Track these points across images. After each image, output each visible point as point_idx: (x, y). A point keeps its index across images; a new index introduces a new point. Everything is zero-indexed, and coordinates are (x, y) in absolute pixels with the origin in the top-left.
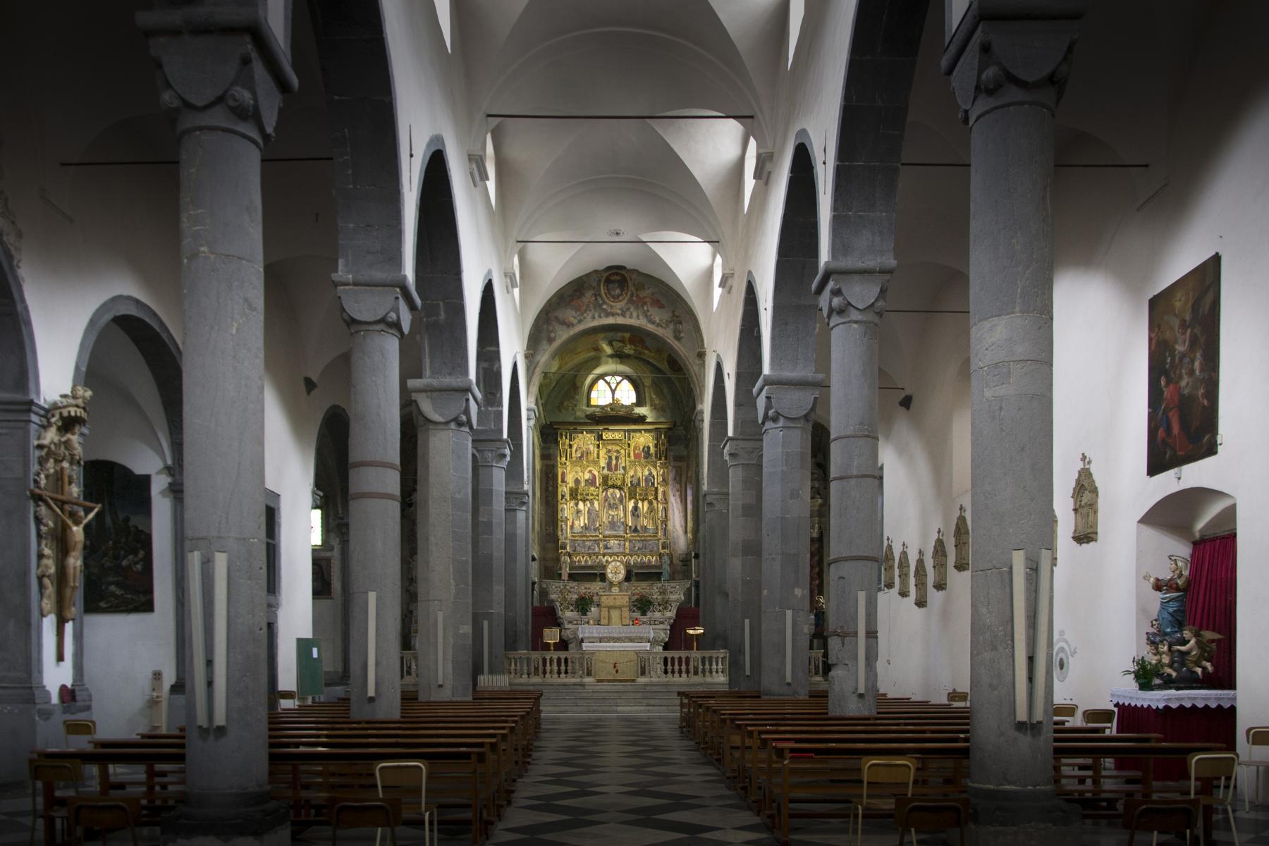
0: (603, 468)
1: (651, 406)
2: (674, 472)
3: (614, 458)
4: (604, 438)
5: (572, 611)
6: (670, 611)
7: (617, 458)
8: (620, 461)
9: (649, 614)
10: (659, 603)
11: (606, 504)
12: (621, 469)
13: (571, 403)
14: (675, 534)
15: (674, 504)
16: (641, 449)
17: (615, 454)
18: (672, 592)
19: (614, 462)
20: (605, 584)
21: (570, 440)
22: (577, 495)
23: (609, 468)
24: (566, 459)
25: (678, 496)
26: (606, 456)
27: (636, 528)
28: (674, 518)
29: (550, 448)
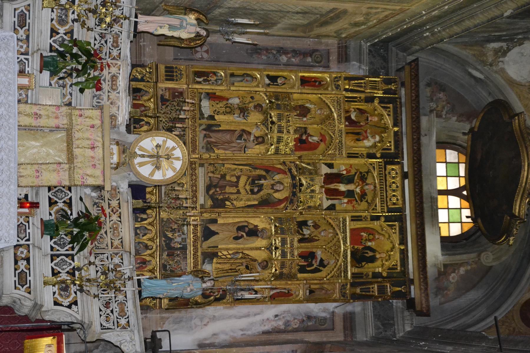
0: (330, 166)
1: (445, 266)
2: (324, 315)
3: (351, 187)
4: (389, 167)
5: (54, 32)
6: (56, 303)
7: (350, 194)
8: (346, 200)
9: (47, 242)
10: (79, 269)
11: (259, 172)
12: (330, 202)
13: (443, 107)
14: (197, 321)
15: (259, 318)
16: (369, 244)
17: (358, 190)
18: (107, 305)
19: (343, 188)
20: (123, 129)
21: (382, 100)
22: (278, 107)
23: (330, 178)
24: (346, 90)
25: (274, 324)
26: (353, 172)
27: (214, 233)
28: (230, 317)
29: (360, 61)
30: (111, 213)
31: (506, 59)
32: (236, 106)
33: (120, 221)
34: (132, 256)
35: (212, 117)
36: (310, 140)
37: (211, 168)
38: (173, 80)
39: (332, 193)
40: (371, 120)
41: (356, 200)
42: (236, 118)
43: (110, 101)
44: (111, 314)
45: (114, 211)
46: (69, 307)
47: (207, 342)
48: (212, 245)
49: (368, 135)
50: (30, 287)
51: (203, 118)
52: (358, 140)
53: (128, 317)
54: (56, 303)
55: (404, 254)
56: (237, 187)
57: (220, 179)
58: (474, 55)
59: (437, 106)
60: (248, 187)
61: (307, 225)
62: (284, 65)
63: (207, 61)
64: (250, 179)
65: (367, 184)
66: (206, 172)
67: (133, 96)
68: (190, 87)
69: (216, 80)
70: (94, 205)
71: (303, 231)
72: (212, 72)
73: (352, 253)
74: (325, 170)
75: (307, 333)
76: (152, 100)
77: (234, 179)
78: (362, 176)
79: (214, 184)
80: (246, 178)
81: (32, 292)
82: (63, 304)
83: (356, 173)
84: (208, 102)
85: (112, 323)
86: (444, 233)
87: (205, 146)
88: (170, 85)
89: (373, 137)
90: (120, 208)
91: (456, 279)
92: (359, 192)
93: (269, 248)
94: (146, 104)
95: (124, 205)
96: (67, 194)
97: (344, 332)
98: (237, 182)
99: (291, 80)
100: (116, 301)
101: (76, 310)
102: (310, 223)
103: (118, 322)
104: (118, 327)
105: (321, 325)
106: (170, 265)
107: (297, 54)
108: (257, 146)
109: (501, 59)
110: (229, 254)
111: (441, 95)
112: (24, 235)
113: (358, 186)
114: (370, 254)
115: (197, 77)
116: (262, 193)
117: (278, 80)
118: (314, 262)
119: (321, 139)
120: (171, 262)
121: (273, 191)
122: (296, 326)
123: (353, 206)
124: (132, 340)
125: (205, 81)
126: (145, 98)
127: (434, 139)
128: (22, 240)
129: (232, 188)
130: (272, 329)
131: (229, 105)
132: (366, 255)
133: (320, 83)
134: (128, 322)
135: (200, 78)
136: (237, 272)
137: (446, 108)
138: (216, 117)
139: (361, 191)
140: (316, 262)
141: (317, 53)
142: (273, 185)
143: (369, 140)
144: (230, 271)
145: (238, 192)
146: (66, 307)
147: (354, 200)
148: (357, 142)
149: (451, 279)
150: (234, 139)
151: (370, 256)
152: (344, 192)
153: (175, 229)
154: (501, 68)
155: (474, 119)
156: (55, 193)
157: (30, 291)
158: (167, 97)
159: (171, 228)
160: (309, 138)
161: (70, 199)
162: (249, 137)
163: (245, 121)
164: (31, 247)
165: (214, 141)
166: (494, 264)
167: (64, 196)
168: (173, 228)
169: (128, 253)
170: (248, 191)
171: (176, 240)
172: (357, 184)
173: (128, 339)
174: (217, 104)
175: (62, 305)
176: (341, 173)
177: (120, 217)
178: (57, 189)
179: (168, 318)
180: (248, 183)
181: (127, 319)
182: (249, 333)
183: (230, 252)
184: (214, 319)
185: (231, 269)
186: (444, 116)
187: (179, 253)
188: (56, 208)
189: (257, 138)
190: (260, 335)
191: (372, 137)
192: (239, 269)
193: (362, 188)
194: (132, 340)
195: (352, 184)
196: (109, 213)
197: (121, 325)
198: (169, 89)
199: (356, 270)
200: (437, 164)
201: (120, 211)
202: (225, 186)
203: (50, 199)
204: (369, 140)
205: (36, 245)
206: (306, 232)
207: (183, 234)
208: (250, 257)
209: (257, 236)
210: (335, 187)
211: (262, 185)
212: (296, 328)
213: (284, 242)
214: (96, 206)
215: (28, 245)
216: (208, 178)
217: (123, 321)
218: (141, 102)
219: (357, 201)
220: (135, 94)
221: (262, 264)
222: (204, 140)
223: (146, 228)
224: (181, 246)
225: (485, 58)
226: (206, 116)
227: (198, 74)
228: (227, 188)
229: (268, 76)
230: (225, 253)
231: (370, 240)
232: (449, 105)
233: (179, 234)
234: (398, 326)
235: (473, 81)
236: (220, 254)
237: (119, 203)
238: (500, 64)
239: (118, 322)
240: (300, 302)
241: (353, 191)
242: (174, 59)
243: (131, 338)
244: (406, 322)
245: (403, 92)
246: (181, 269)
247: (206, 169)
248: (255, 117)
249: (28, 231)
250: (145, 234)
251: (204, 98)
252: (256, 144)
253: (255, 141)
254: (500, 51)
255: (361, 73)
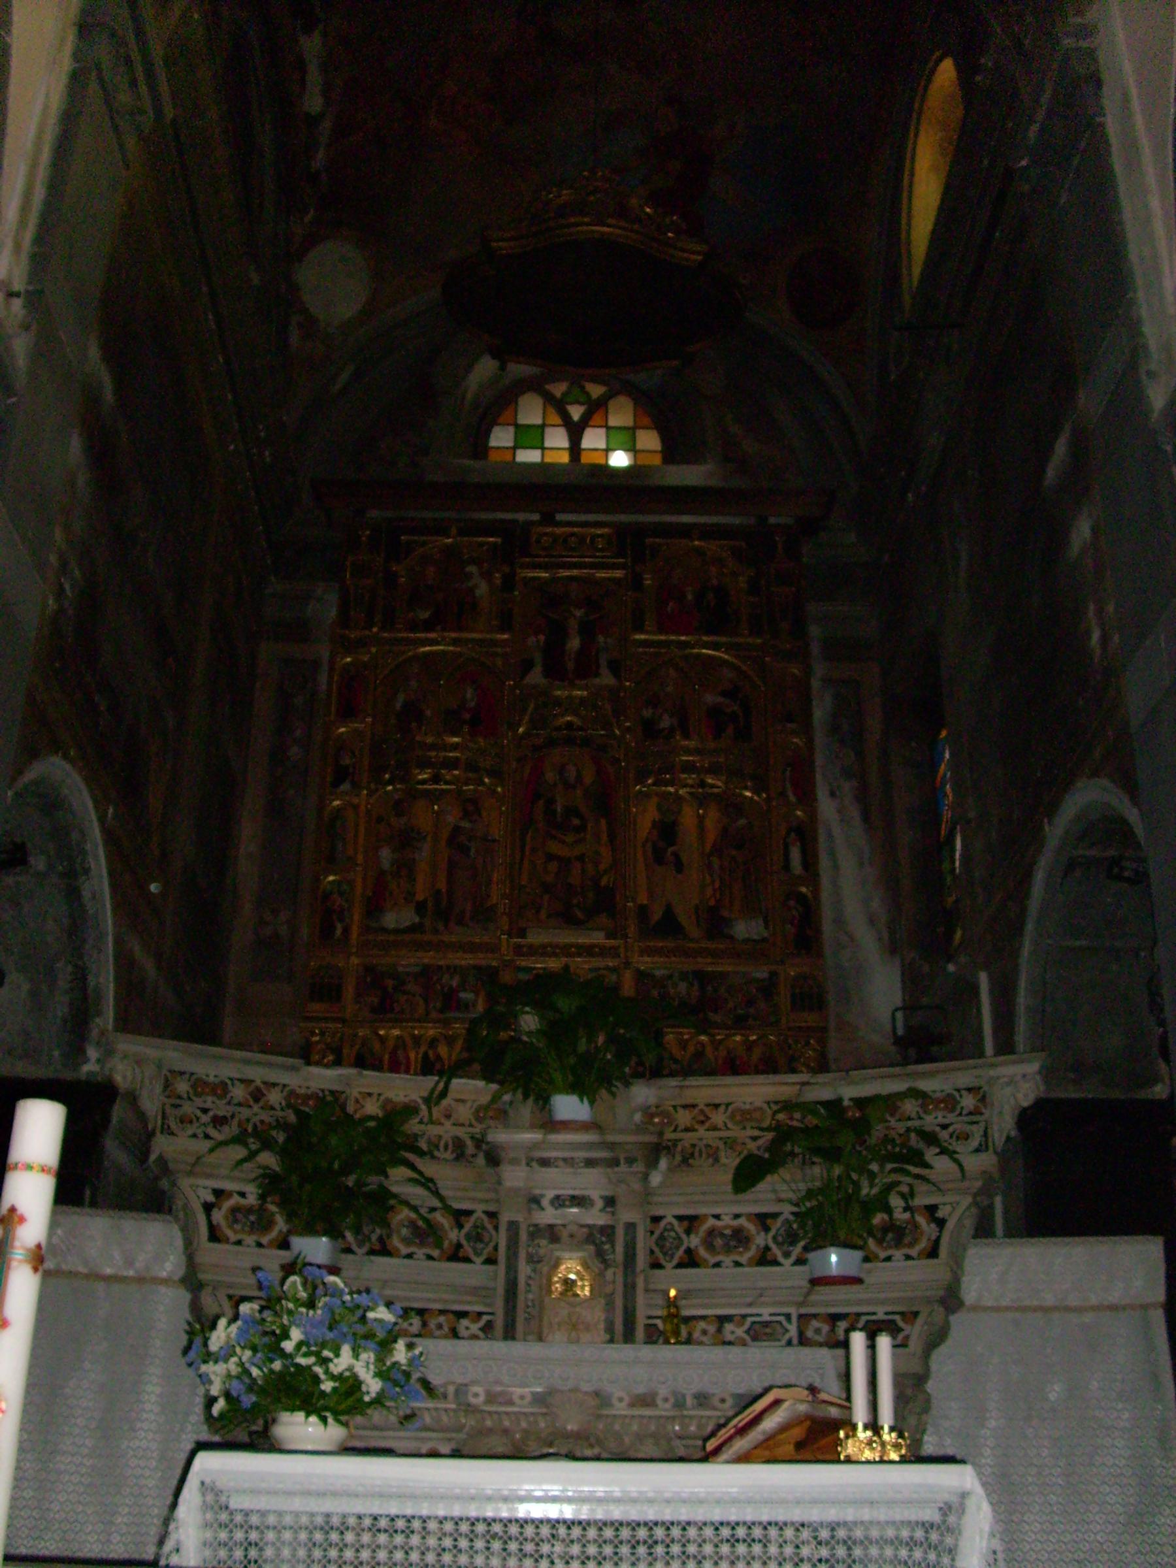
0: (527, 666)
6: (933, 1253)
7: (588, 631)
12: (604, 670)
17: (579, 613)
19: (574, 643)
23: (554, 671)
27: (669, 914)
30: (707, 1125)
33: (728, 1105)
34: (812, 1081)
35: (420, 908)
36: (473, 704)
39: (586, 668)
42: (423, 854)
43: (443, 1120)
44: (951, 1129)
45: (702, 1118)
46: (941, 1223)
47: (886, 936)
50: (902, 1314)
51: (421, 925)
53: (958, 1090)
54: (933, 1253)
55: (708, 532)
60: (570, 839)
68: (354, 950)
69: (341, 894)
70: (689, 1165)
71: (664, 729)
73: (709, 632)
74: (536, 677)
76: (382, 1032)
77: (553, 866)
81: (915, 1309)
82: (933, 1237)
85: (974, 1128)
86: (657, 460)
88: (349, 993)
89: (469, 576)
90: (694, 1106)
93: (702, 801)
94: (391, 1044)
95: (690, 1096)
96: (669, 1227)
98: (559, 859)
100: (920, 1118)
101: (948, 1208)
102: (647, 713)
103: (970, 1113)
104: (981, 1114)
108: (484, 814)
110: (713, 882)
112: (778, 1327)
120: (731, 1005)
122: (852, 754)
124: (1011, 1082)
125: (342, 920)
126: (377, 1046)
127: (469, 463)
128: (787, 1331)
134: (969, 1090)
138: (420, 897)
145: (581, 858)
146: (940, 1232)
156: (665, 1254)
157: (912, 1313)
161: (680, 1218)
163: (429, 839)
164: (803, 1311)
167: (673, 1234)
169: (804, 1088)
173: (1008, 1090)
175: (937, 1241)
176: (542, 644)
177: (717, 1106)
178: (657, 1250)
181: (964, 1093)
183: (708, 879)
184: (839, 921)
188: (702, 1252)
189: (466, 815)
194: (1011, 1082)
196: (708, 1130)
197: (976, 1107)
201: (701, 1106)
203: (680, 1265)
205: (801, 1299)
206: (666, 722)
207: (670, 977)
209: (674, 823)
213: (689, 768)
214: (690, 1161)
215: (801, 1316)
217: (968, 1102)
218: (387, 1057)
226: (417, 920)
227: (326, 931)
230: (709, 892)
236: (712, 903)
237: (685, 1107)
239: (970, 1113)
240: (810, 741)
243: (1008, 1084)
245: (374, 514)
248: (422, 817)
249: (766, 1318)
252: (480, 815)
255: (333, 597)
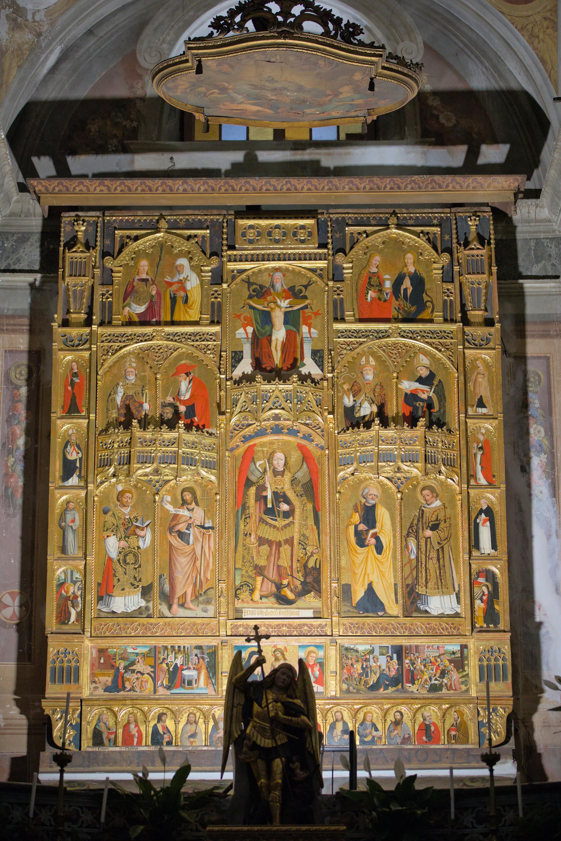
16: (388, 285)
17: (284, 304)
26: (248, 313)
27: (370, 591)
31: (29, 7)
32: (123, 543)
36: (187, 396)
37: (244, 595)
38: (77, 669)
40: (147, 274)
41: (302, 309)
48: (393, 595)
49: (176, 280)
52: (186, 300)
56: (279, 544)
57: (264, 576)
58: (19, 67)
59: (115, 136)
60: (281, 522)
61: (353, 407)
62: (36, 442)
63: (31, 596)
64: (265, 517)
65: (273, 286)
66: (251, 604)
67: (110, 746)
72: (59, 593)
75: (553, 409)
78: (257, 296)
79: (274, 589)
80: (262, 526)
83: (251, 307)
84: (117, 598)
87: (201, 606)
91: (449, 114)
92: (287, 301)
97: (552, 337)
98: (269, 543)
99: (70, 432)
105: (540, 382)
106: (430, 679)
107: (14, 415)
109: (30, 17)
111: (93, 128)
113: (275, 303)
114: (407, 284)
115: (69, 621)
116: (291, 494)
117: (70, 457)
118: (424, 396)
119: (184, 375)
120: (426, 677)
121: (287, 472)
122: (542, 430)
123: (316, 314)
129: (282, 555)
130: (547, 478)
131: (121, 557)
132: (409, 292)
133: (75, 375)
135: (70, 614)
136: (442, 547)
137: (118, 120)
139: (286, 298)
140: (423, 391)
141: (13, 374)
142: (276, 473)
143: (186, 279)
144: (441, 561)
145: (290, 541)
147: (304, 313)
148: (190, 302)
149: (450, 124)
150: (188, 549)
151: (411, 284)
152: (288, 332)
153: (362, 668)
154: (46, 16)
155: (140, 66)
158: (110, 679)
159: (360, 675)
160: (182, 398)
162: (183, 519)
165: (191, 587)
166: (420, 39)
168: (360, 671)
170: (287, 521)
171: (384, 667)
172: (272, 305)
174: (119, 580)
176: (250, 336)
179: (526, 679)
180: (273, 522)
182: (554, 522)
185: (438, 560)
186: (135, 124)
187: (407, 661)
190: (558, 502)
191: (180, 272)
192: (439, 543)
193: (278, 295)
195: (273, 314)
198: (93, 675)
199: (438, 315)
200: (224, 138)
202: (279, 567)
204: (186, 279)
207: (372, 651)
208: (415, 522)
210: (279, 348)
211: (275, 494)
212: (546, 434)
216: (264, 600)
218: (120, 731)
219: (306, 307)
220: (106, 741)
221: (427, 498)
222: (190, 609)
223: (361, 724)
224: (395, 656)
225: (26, 46)
226: (143, 603)
228: (281, 563)
229: (66, 476)
231: (381, 284)
232: (113, 114)
233: (371, 660)
234: (540, 232)
235: (67, 66)
236: (409, 581)
238: (37, 18)
241: (286, 314)
242: (30, 660)
244: (532, 216)
246: (439, 656)
247: (245, 605)
250: (374, 725)
251: (108, 605)
253: (191, 507)
254: (15, 20)
